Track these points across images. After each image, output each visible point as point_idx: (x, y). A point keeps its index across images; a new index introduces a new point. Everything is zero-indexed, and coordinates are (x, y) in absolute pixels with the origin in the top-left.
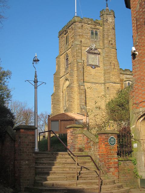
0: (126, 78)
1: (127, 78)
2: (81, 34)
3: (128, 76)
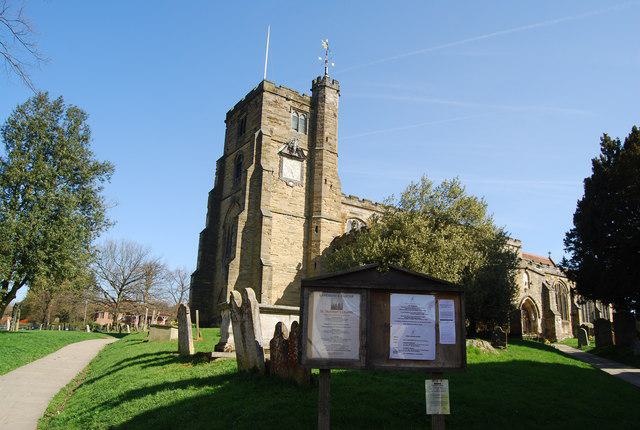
3: (355, 210)
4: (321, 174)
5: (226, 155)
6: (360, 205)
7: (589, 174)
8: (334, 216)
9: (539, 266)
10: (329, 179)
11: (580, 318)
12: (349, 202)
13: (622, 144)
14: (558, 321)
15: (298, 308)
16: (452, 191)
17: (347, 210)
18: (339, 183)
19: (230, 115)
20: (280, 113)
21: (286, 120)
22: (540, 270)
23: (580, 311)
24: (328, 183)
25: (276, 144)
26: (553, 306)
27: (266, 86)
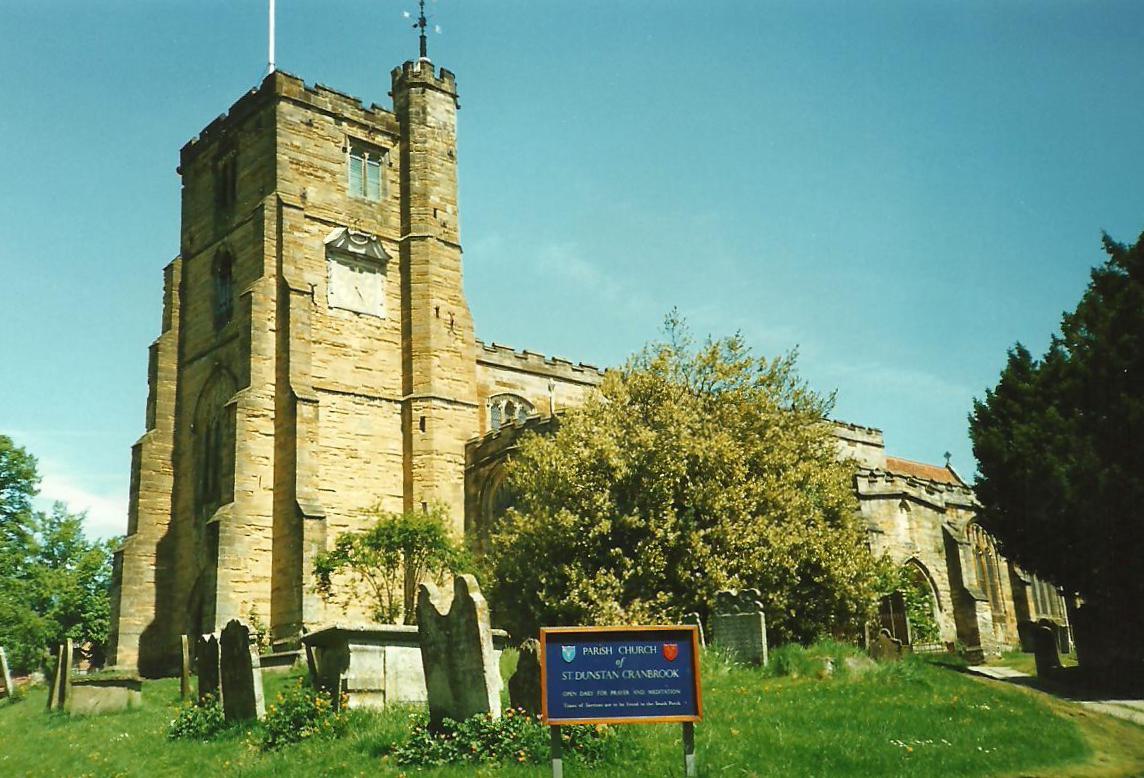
0: (498, 383)
1: (504, 385)
2: (303, 158)
3: (506, 376)
4: (426, 296)
5: (187, 255)
6: (518, 365)
7: (485, 668)
8: (464, 393)
9: (931, 491)
10: (445, 306)
11: (1031, 605)
12: (495, 358)
13: (982, 476)
14: (984, 613)
15: (415, 628)
16: (485, 381)
17: (487, 376)
18: (467, 316)
19: (189, 153)
20: (320, 151)
21: (335, 167)
22: (936, 499)
23: (1029, 589)
24: (444, 315)
25: (316, 227)
26: (970, 578)
27: (284, 88)
